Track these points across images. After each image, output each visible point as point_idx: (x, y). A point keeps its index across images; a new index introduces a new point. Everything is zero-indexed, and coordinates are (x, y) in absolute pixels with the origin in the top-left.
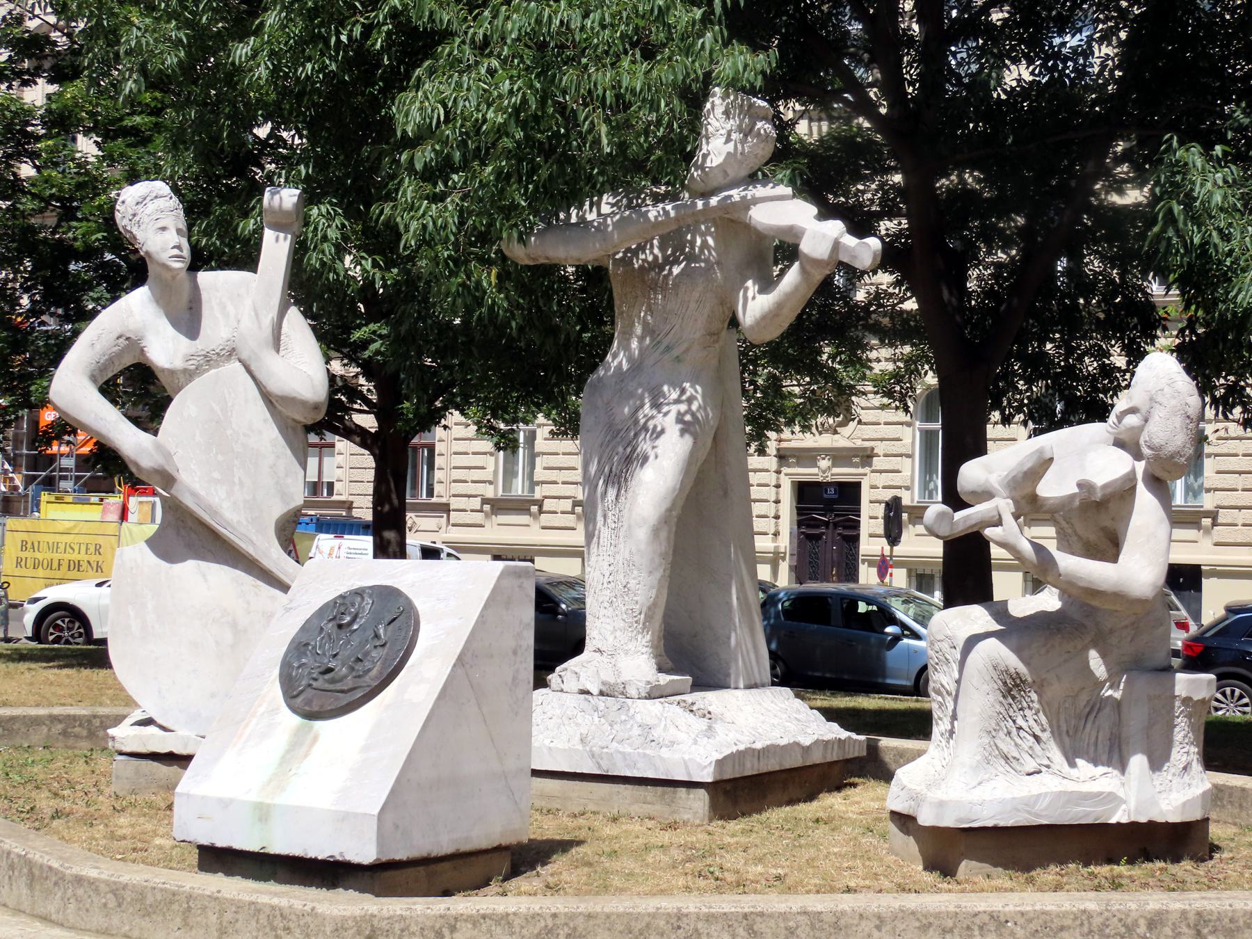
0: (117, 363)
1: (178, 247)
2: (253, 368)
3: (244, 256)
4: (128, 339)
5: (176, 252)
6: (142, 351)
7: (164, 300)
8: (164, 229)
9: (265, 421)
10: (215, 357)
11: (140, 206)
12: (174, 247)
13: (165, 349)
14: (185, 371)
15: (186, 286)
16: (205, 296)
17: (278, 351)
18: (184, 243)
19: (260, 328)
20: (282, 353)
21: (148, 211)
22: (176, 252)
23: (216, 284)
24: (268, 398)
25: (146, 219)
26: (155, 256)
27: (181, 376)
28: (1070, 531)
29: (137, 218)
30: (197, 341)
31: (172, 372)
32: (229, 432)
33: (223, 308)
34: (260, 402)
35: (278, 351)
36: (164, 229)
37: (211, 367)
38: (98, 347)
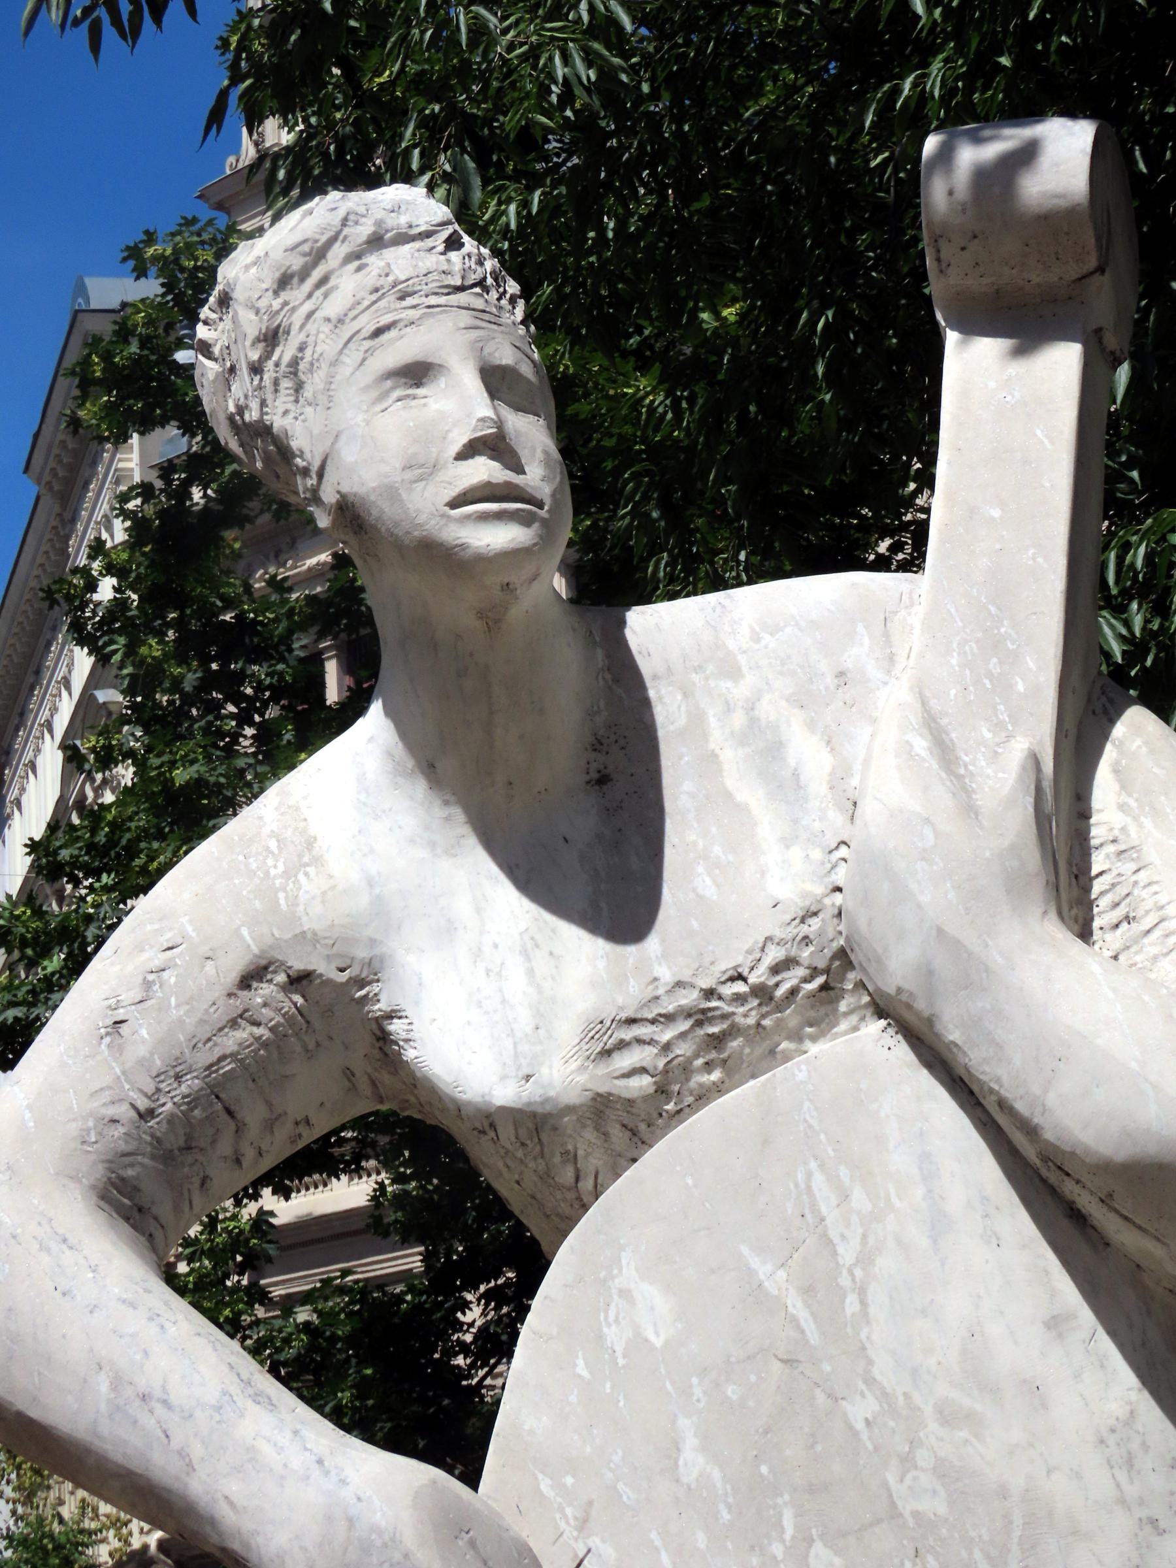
0: (253, 1114)
1: (494, 445)
2: (952, 1032)
3: (849, 498)
4: (299, 981)
5: (484, 470)
6: (382, 1042)
7: (464, 768)
8: (417, 373)
9: (1056, 1324)
10: (747, 1015)
11: (296, 295)
12: (470, 450)
13: (493, 1001)
14: (600, 1107)
15: (567, 664)
16: (668, 710)
17: (1085, 933)
18: (533, 435)
19: (969, 810)
20: (1107, 940)
21: (334, 306)
22: (484, 470)
23: (720, 653)
24: (1053, 1186)
25: (326, 344)
26: (383, 511)
27: (585, 1142)
28: (843, 1172)
29: (285, 352)
30: (652, 943)
31: (535, 1125)
32: (860, 1409)
33: (768, 751)
34: (1018, 1224)
35: (1085, 933)
36: (417, 373)
37: (735, 1073)
38: (143, 1036)
